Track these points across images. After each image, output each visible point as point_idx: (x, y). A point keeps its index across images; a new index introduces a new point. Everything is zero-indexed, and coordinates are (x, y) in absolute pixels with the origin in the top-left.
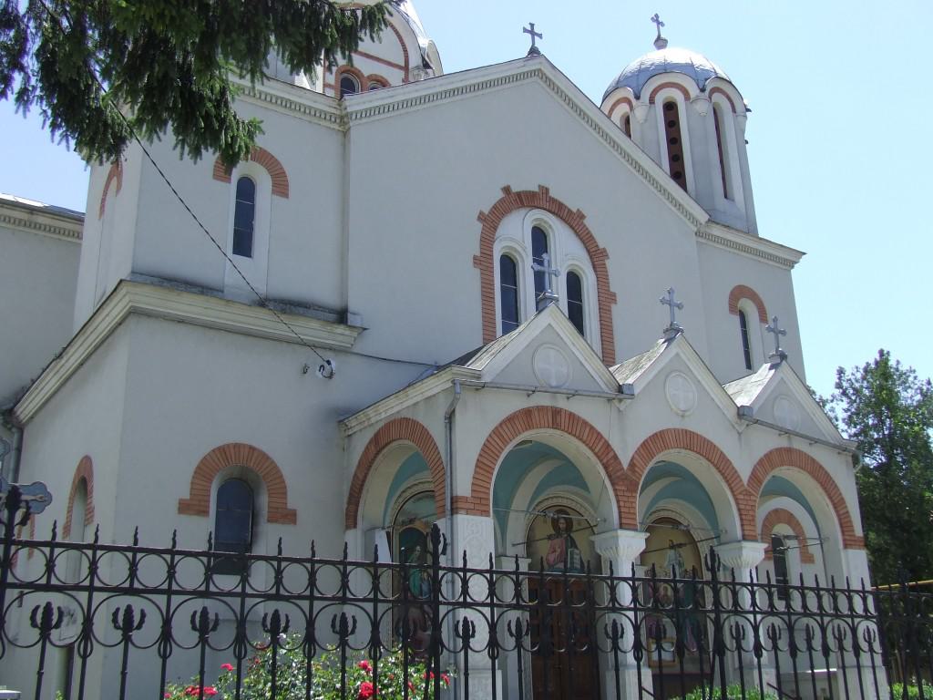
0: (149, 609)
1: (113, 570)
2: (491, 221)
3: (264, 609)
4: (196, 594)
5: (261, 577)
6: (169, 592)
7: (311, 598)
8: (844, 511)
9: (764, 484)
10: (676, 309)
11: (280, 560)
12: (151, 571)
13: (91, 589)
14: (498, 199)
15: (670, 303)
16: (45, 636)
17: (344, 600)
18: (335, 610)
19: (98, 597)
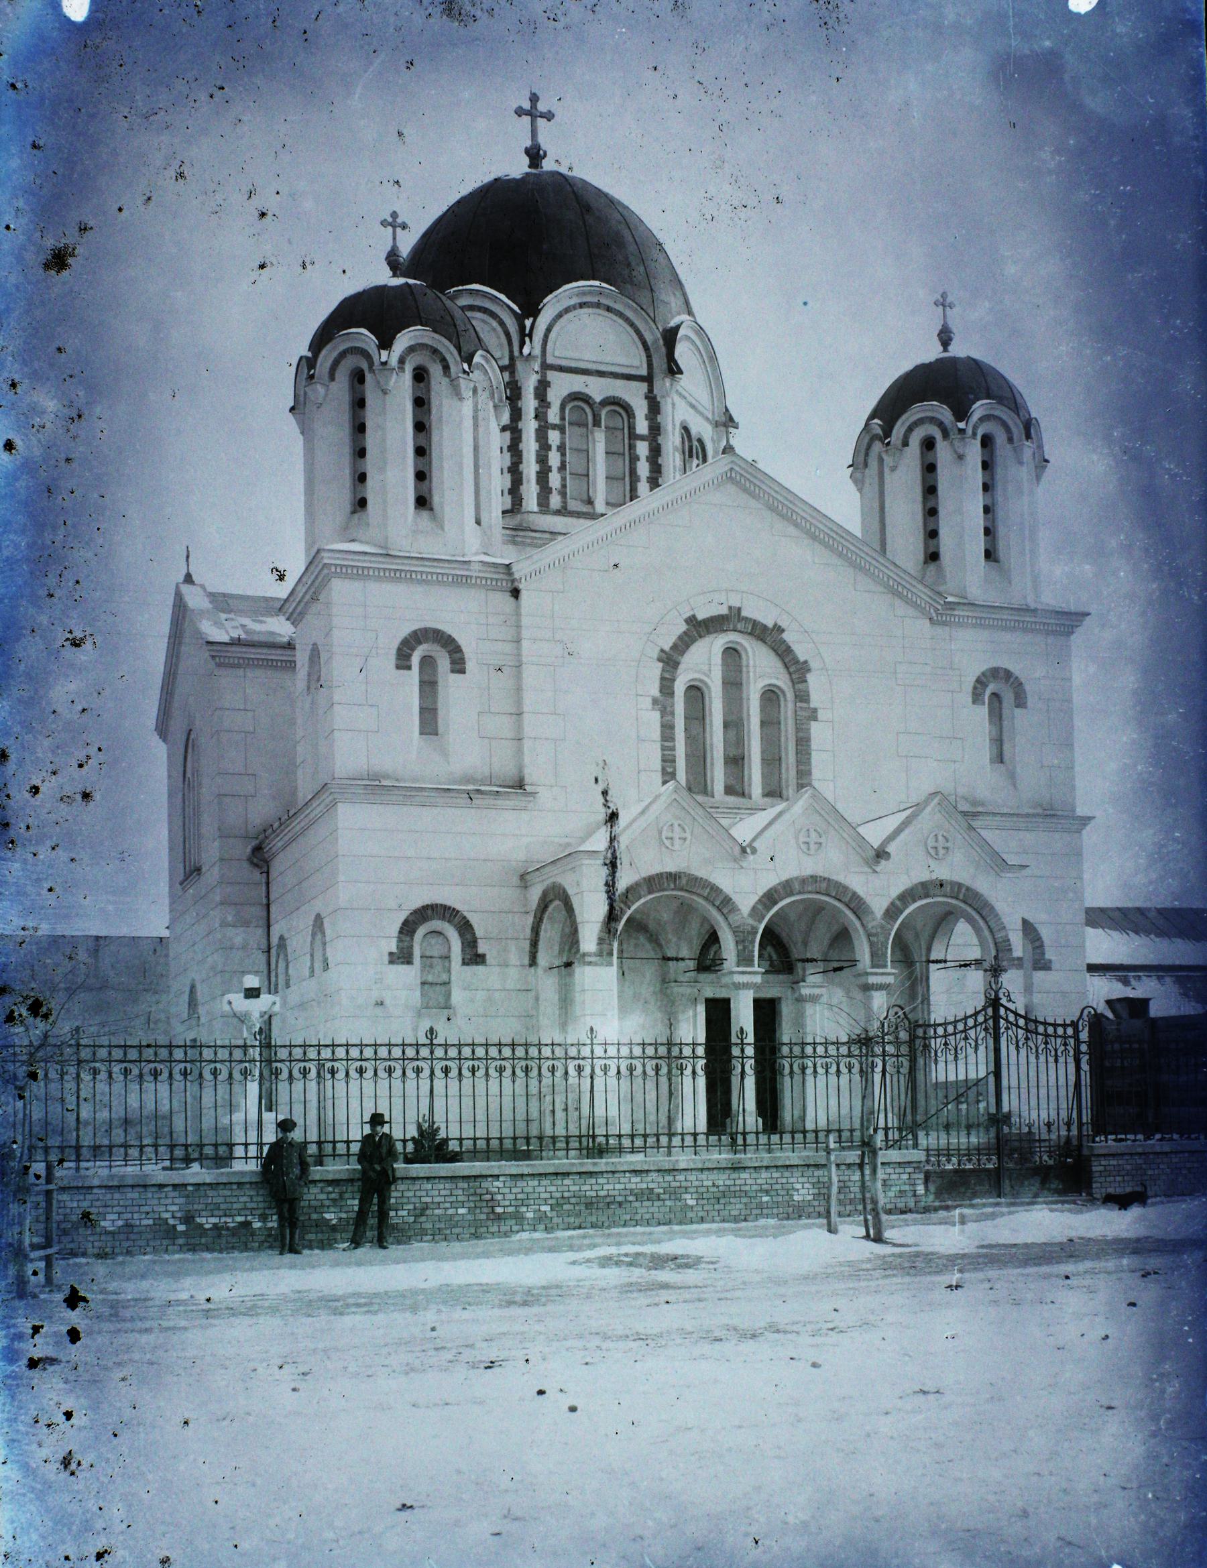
0: (482, 1066)
1: (297, 1053)
2: (670, 661)
3: (329, 1065)
4: (211, 1061)
5: (439, 1052)
6: (347, 1060)
7: (540, 1059)
8: (721, 898)
9: (633, 908)
10: (399, 230)
11: (460, 1045)
12: (369, 1052)
13: (231, 1061)
14: (764, 622)
15: (394, 226)
16: (185, 1078)
17: (802, 1057)
18: (800, 1061)
19: (143, 1064)
